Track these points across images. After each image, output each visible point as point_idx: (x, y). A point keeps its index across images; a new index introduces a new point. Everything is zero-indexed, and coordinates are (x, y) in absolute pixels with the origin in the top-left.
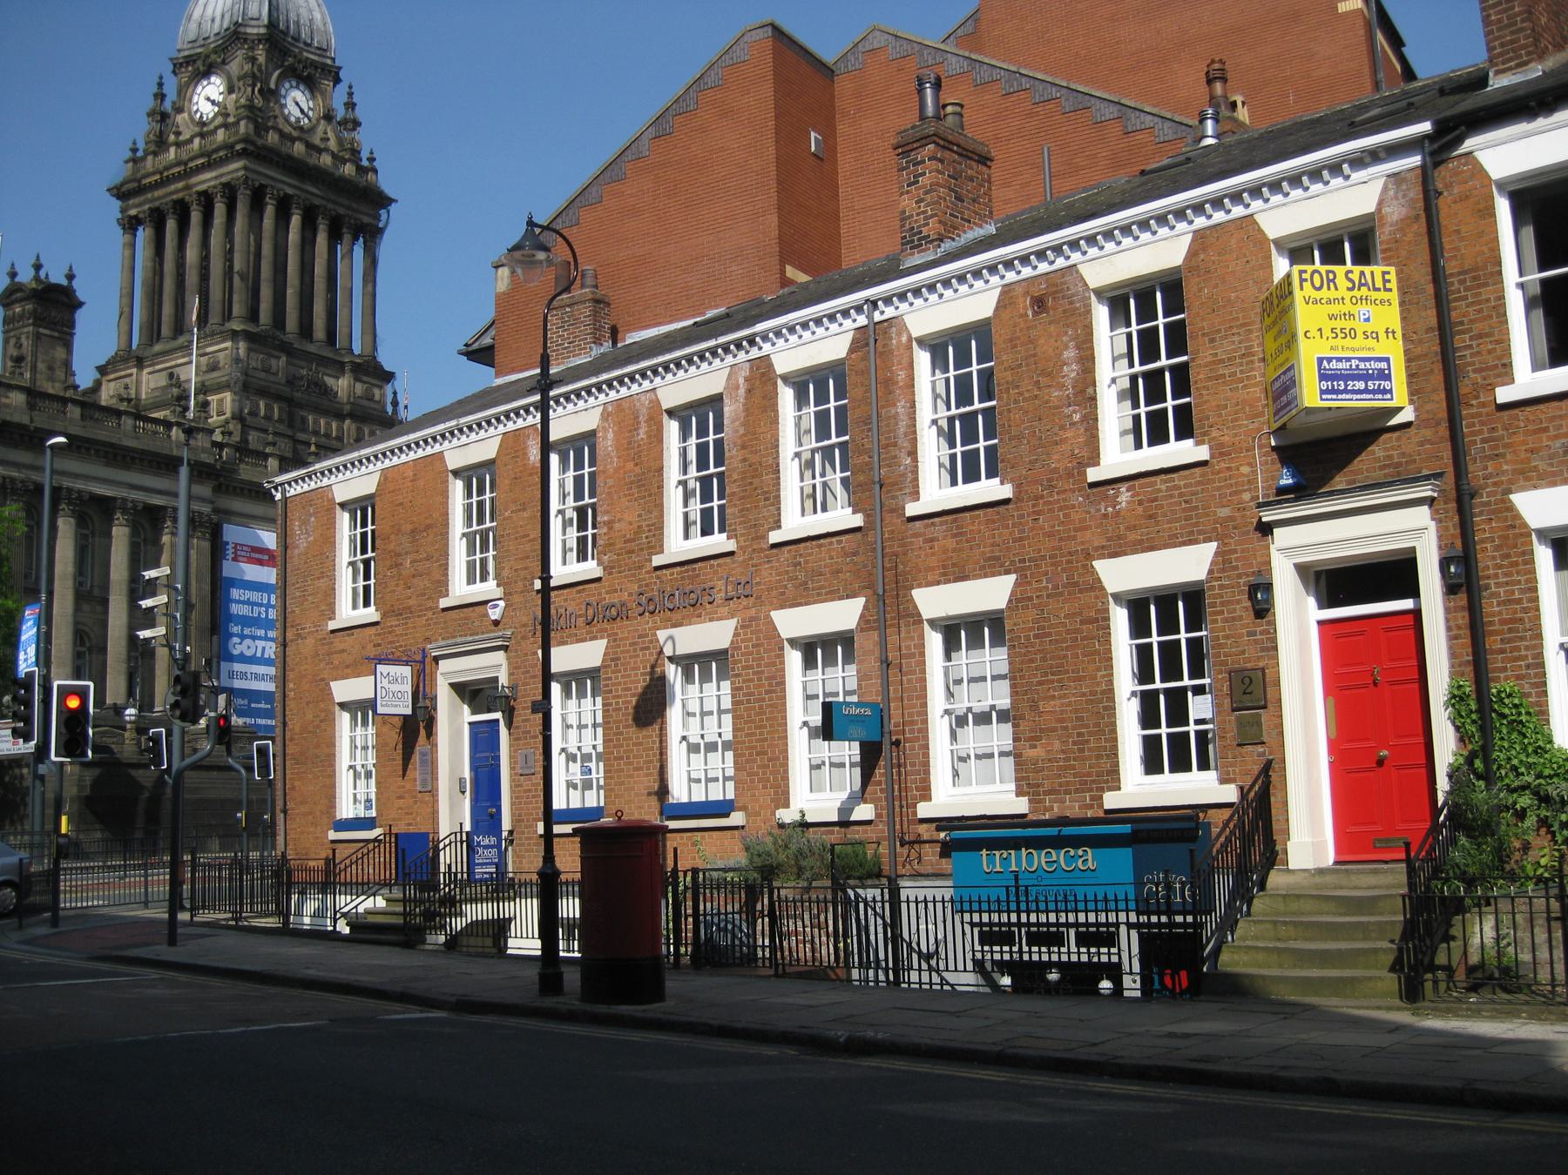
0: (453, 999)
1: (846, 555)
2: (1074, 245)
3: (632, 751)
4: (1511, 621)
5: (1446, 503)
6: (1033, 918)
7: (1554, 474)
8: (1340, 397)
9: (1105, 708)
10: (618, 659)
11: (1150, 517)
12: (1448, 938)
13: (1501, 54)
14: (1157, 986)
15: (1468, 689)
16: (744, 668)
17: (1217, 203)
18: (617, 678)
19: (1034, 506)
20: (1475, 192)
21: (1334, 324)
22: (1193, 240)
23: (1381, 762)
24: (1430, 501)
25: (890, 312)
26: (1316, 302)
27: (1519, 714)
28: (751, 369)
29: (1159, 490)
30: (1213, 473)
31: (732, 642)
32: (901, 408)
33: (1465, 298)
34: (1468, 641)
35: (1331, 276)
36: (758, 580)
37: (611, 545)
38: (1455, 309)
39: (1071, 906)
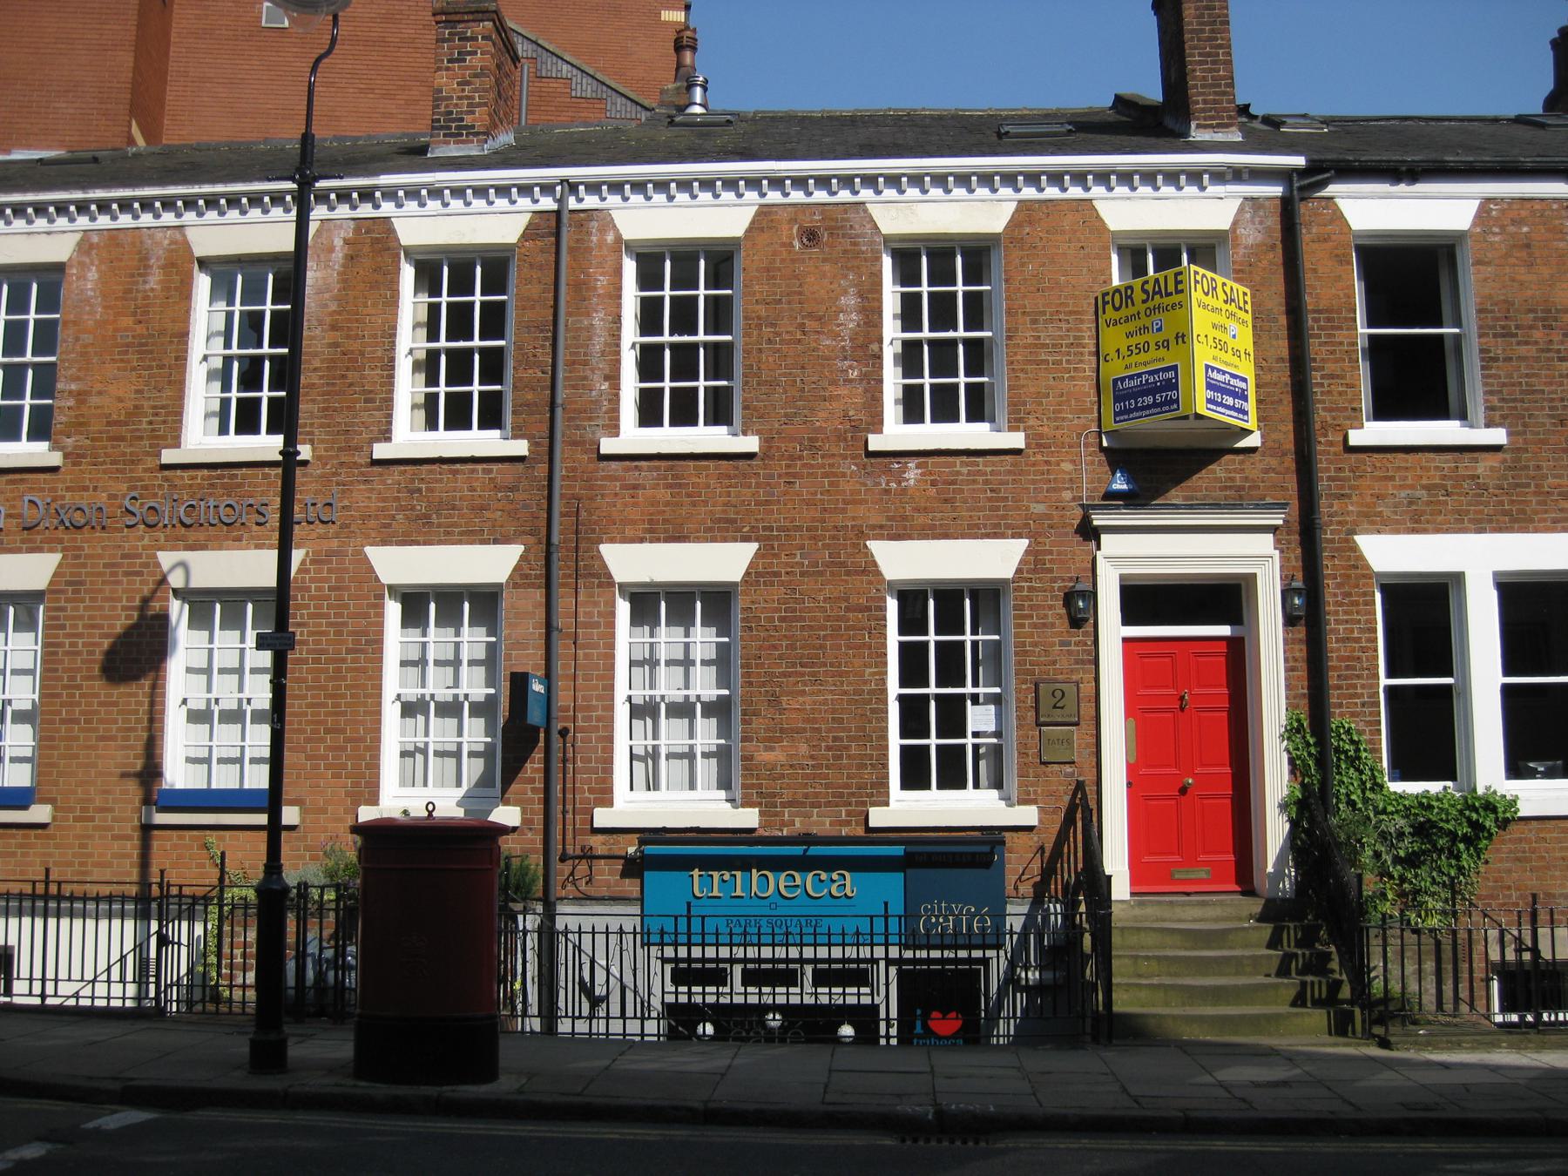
0: (117, 1086)
1: (496, 488)
2: (870, 181)
3: (97, 712)
4: (1349, 658)
6: (683, 952)
7: (1397, 522)
9: (873, 711)
10: (82, 583)
11: (946, 501)
14: (919, 1029)
16: (311, 616)
17: (1056, 178)
18: (76, 609)
19: (788, 466)
22: (1017, 211)
23: (1184, 790)
24: (1273, 529)
25: (591, 202)
28: (357, 230)
29: (958, 473)
30: (1027, 465)
31: (51, 583)
32: (598, 320)
36: (346, 503)
37: (81, 424)
39: (809, 939)
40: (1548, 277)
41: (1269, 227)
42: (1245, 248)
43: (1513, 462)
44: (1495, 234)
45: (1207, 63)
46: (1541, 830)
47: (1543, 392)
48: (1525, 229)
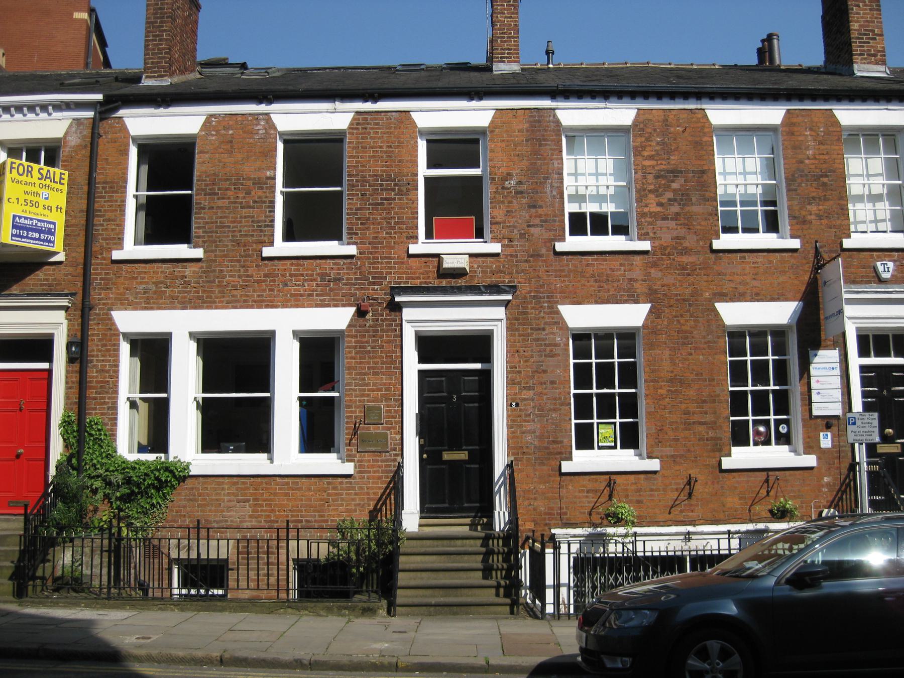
4: (102, 382)
5: (75, 311)
7: (137, 303)
8: (23, 240)
12: (44, 561)
13: (151, 68)
15: (73, 418)
20: (121, 140)
21: (27, 197)
23: (18, 456)
24: (66, 309)
26: (18, 182)
27: (100, 435)
33: (104, 197)
34: (77, 390)
35: (30, 169)
38: (98, 202)
40: (240, 159)
41: (85, 135)
44: (213, 135)
45: (156, 40)
47: (229, 227)
48: (231, 132)
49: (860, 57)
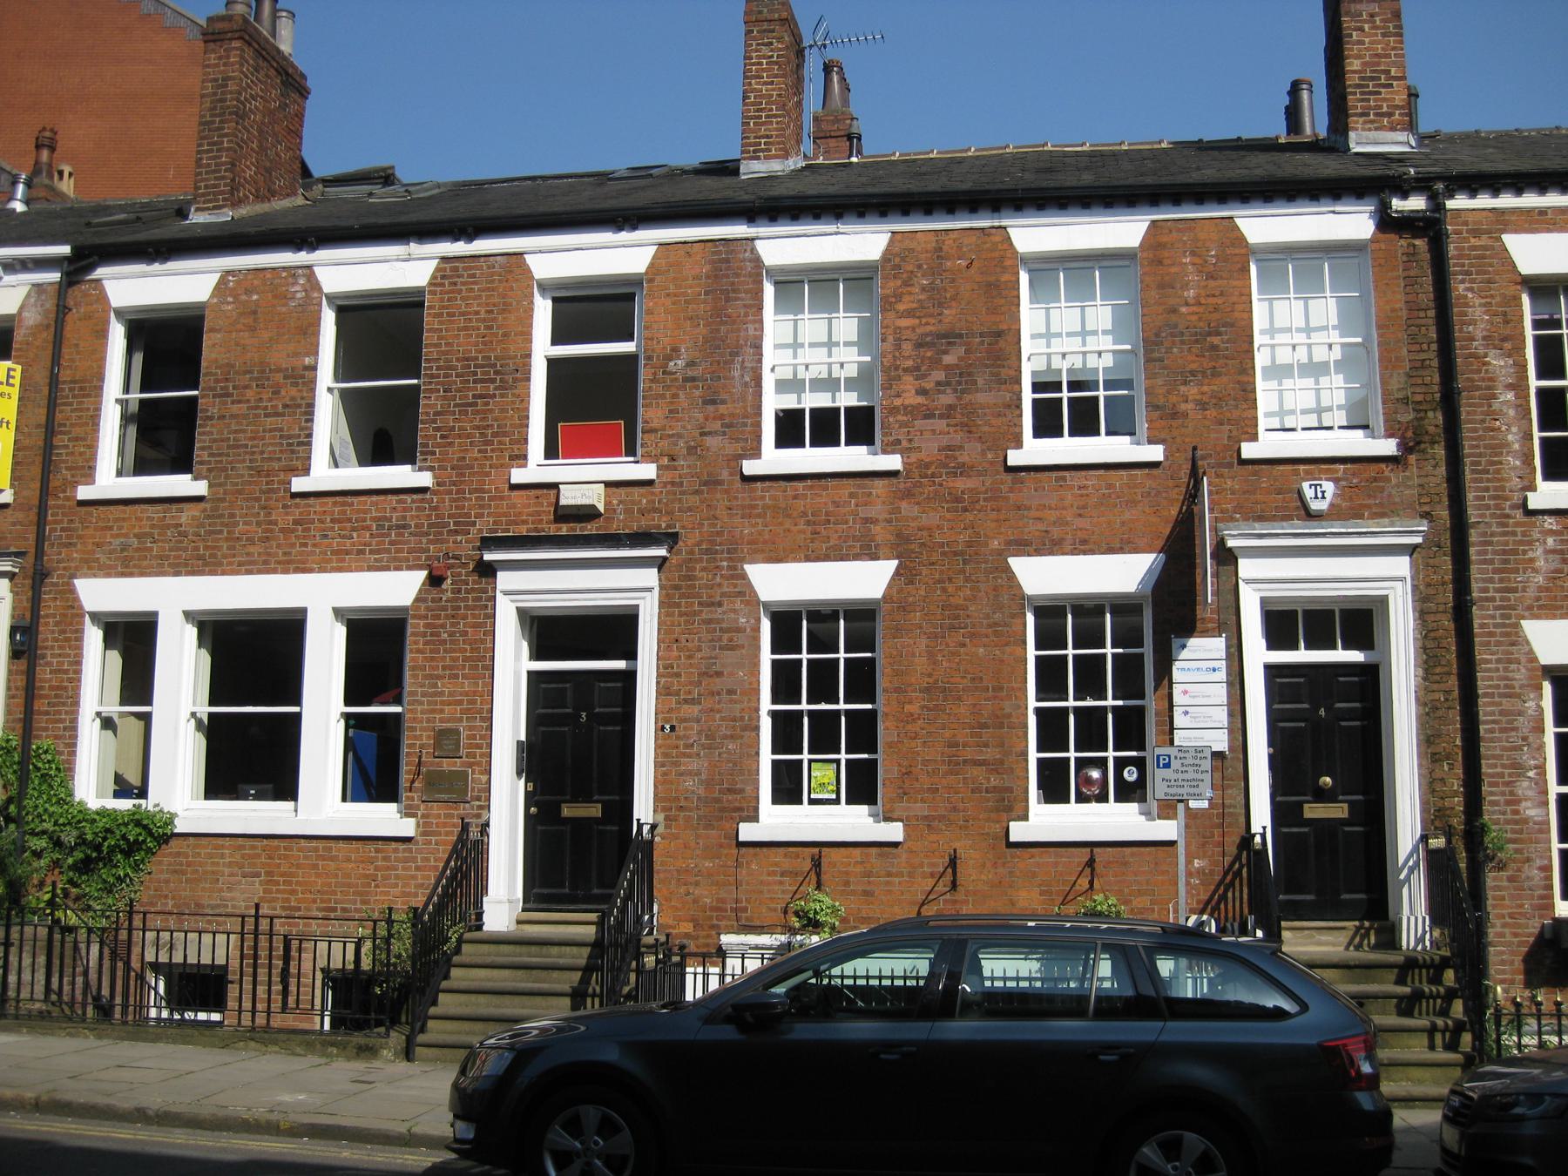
4: (58, 688)
5: (24, 579)
7: (110, 567)
13: (203, 195)
33: (71, 404)
38: (61, 412)
42: (27, 329)
43: (212, 510)
44: (229, 303)
46: (196, 846)
47: (246, 446)
48: (255, 297)
49: (1361, 120)
